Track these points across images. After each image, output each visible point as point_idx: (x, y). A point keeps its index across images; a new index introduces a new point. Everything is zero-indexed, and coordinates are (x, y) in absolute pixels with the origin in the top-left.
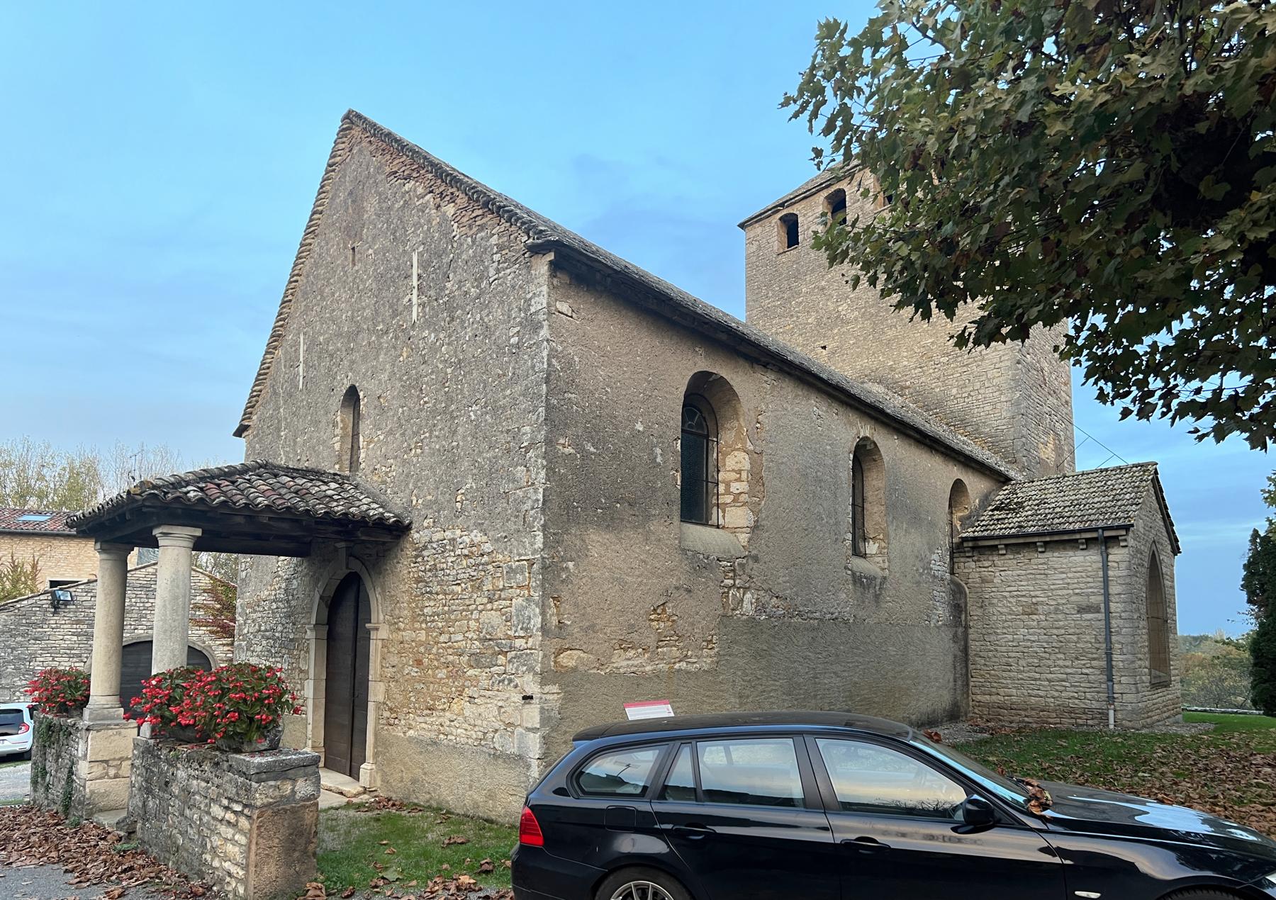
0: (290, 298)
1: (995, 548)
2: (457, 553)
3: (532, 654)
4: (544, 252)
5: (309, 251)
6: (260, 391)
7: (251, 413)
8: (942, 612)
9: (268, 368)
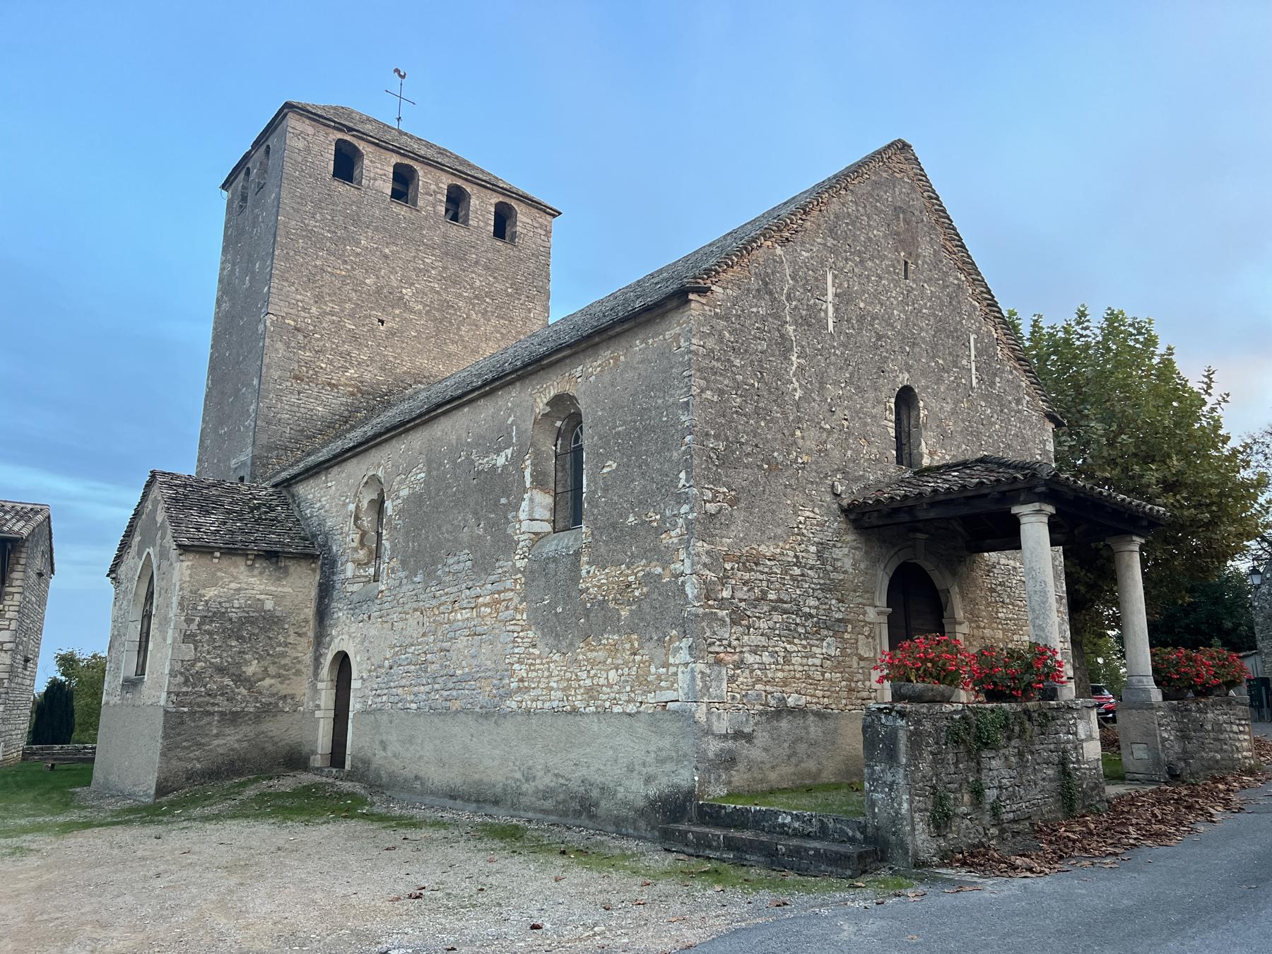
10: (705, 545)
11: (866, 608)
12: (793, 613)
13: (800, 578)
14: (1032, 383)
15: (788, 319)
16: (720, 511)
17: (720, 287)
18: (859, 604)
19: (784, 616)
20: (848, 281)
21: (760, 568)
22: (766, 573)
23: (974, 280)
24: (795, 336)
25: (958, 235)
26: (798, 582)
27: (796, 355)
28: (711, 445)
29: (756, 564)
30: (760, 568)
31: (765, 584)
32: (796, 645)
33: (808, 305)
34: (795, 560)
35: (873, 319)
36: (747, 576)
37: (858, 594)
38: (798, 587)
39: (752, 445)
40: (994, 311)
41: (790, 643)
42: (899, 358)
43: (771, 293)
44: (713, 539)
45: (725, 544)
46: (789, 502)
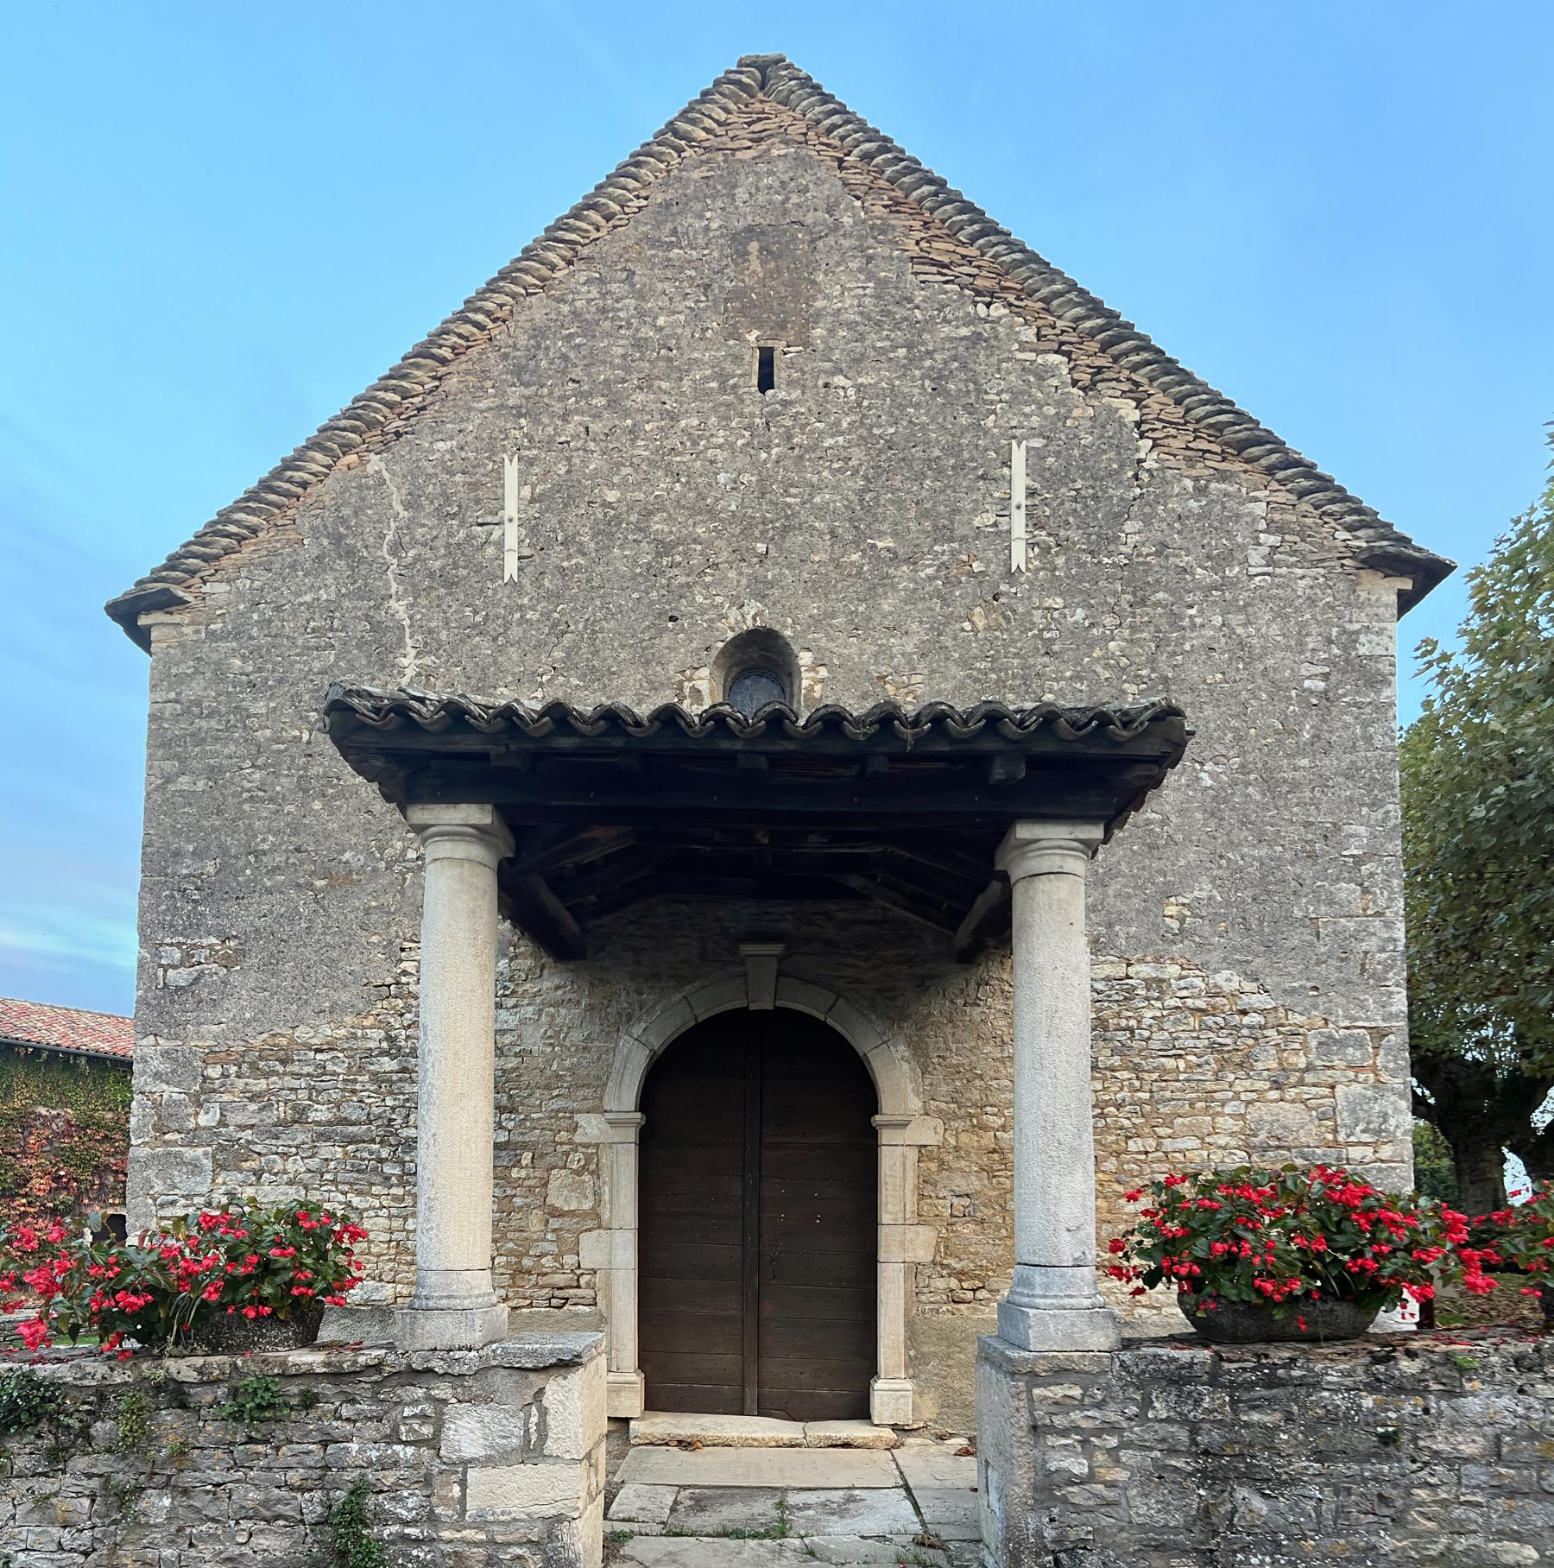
0: (446, 353)
1: (733, 1496)
2: (1166, 1004)
3: (1395, 1168)
4: (1390, 572)
5: (542, 279)
6: (254, 531)
7: (193, 573)
8: (732, 1543)
9: (304, 485)
10: (161, 1041)
11: (577, 1117)
12: (373, 1141)
13: (395, 1077)
14: (1301, 495)
15: (394, 586)
16: (196, 980)
17: (221, 581)
18: (559, 1111)
19: (350, 1148)
20: (569, 459)
21: (295, 1068)
22: (308, 1075)
23: (1046, 300)
24: (411, 618)
25: (968, 208)
26: (391, 1082)
27: (413, 652)
28: (185, 871)
29: (283, 1062)
30: (295, 1068)
31: (303, 1094)
32: (378, 1196)
33: (448, 545)
34: (385, 1045)
35: (648, 514)
36: (261, 1085)
37: (555, 1093)
38: (391, 1093)
39: (287, 851)
40: (1126, 354)
41: (360, 1193)
42: (732, 574)
43: (350, 553)
44: (179, 1030)
45: (207, 1033)
46: (375, 939)
